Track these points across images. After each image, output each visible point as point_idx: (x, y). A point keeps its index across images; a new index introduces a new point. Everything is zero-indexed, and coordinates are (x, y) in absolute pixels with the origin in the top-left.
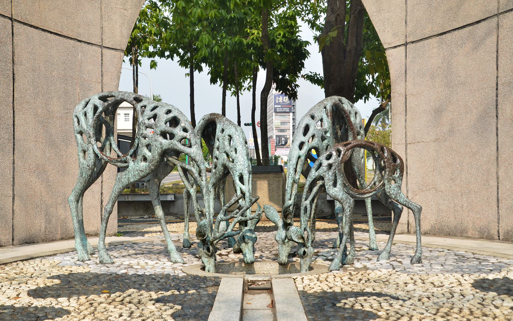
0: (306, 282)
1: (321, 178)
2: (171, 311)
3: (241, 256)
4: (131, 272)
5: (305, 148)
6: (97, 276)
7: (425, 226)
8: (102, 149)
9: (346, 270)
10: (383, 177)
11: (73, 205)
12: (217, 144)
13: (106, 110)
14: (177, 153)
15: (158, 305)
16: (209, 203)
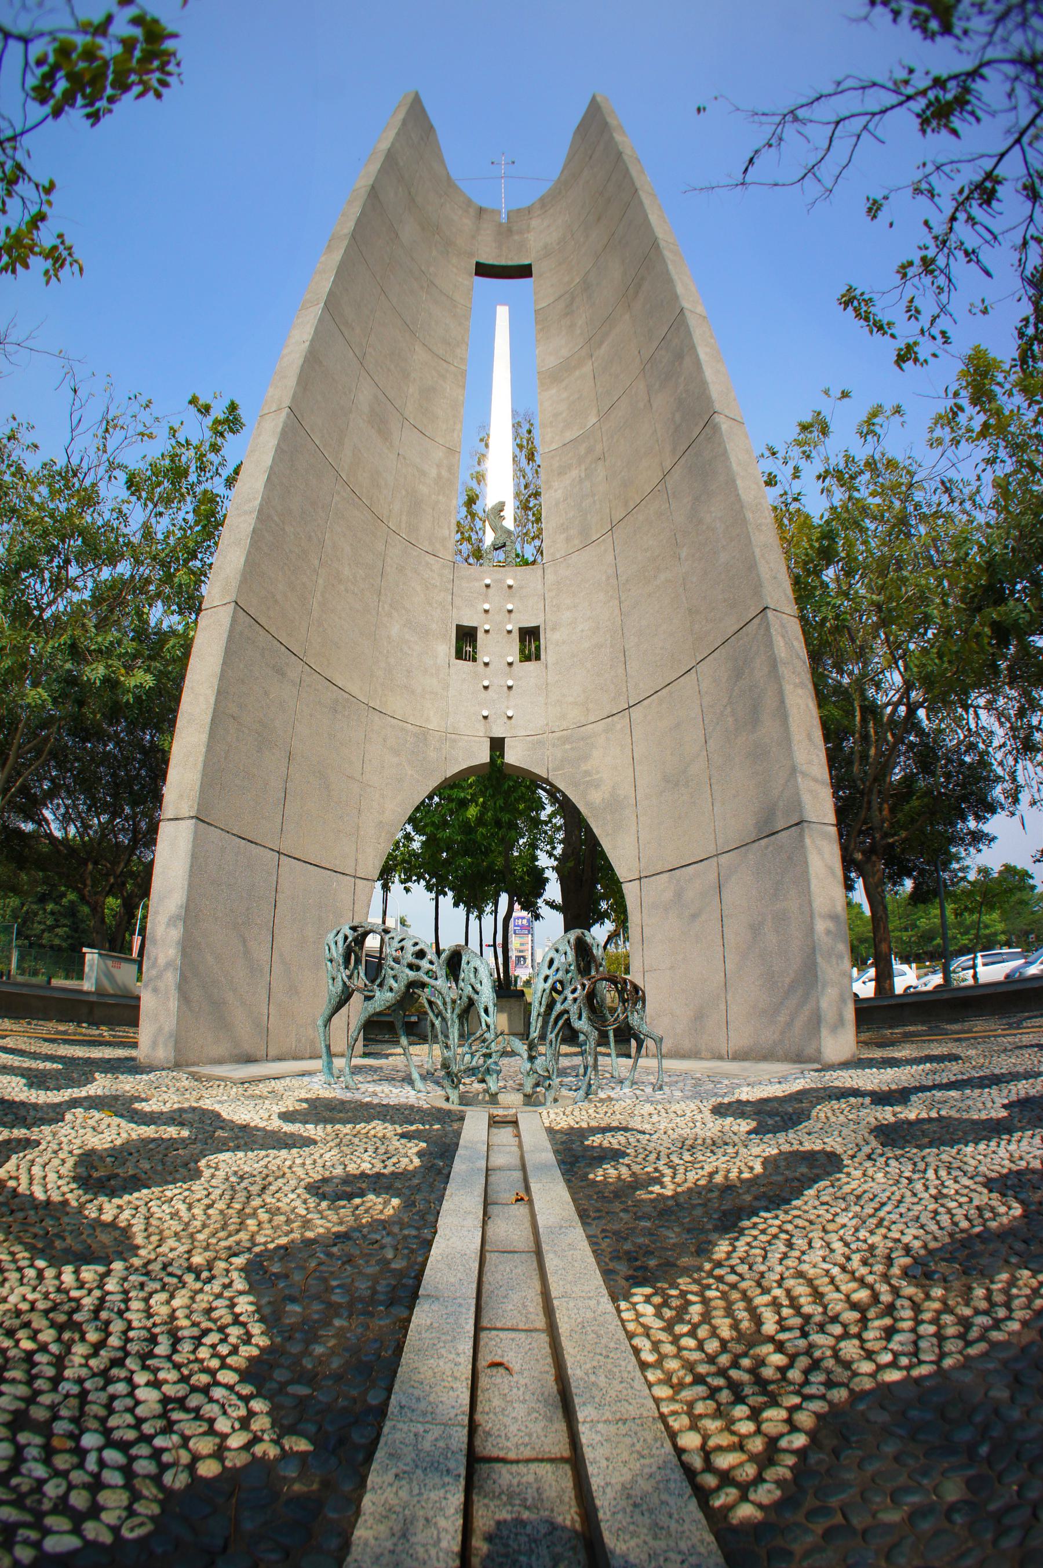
0: (552, 1116)
1: (567, 1012)
2: (415, 1150)
3: (484, 1085)
4: (376, 1101)
5: (550, 981)
6: (343, 1102)
7: (664, 1050)
8: (350, 977)
9: (590, 1101)
10: (626, 1009)
11: (321, 1029)
12: (462, 975)
13: (355, 940)
14: (423, 985)
15: (403, 1141)
16: (454, 1033)
